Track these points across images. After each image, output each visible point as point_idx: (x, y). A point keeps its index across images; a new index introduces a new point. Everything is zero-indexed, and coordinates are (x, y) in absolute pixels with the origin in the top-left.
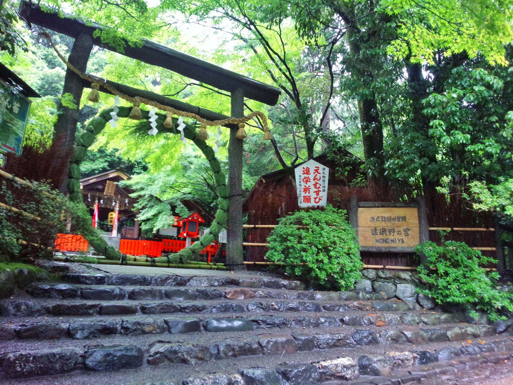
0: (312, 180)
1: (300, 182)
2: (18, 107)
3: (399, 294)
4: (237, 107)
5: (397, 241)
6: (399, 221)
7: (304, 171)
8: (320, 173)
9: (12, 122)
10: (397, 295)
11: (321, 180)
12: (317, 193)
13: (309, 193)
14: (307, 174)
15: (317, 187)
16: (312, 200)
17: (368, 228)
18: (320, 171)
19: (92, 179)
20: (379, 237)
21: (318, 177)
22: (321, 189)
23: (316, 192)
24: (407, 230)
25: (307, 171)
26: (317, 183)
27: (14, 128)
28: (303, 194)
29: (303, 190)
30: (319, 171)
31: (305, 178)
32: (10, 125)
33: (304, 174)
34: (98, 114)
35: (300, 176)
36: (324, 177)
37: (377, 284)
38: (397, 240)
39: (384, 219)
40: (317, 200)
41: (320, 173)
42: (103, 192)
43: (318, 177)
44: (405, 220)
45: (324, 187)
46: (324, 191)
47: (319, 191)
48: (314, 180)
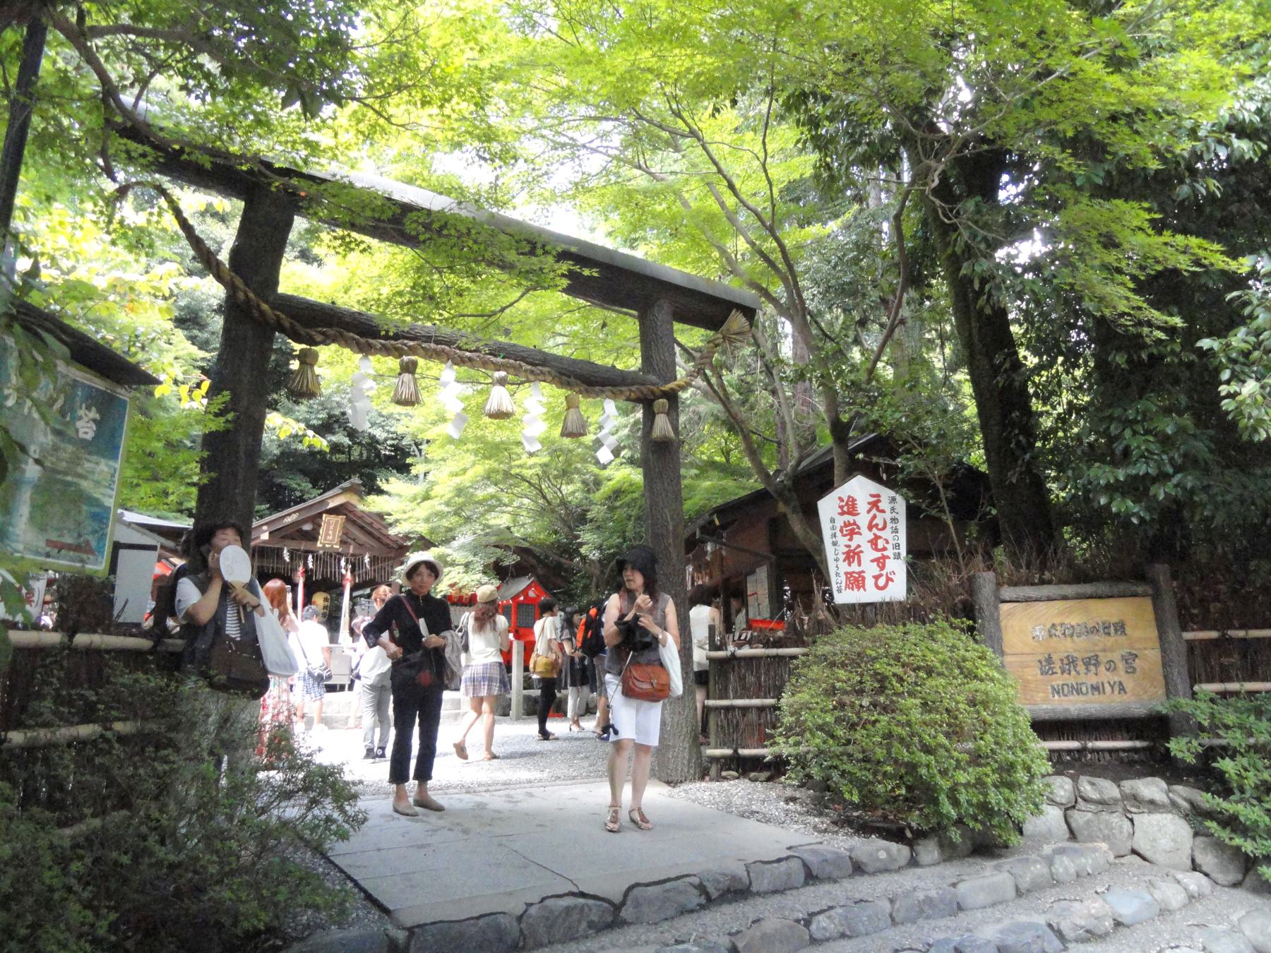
0: (864, 530)
1: (834, 535)
2: (94, 421)
3: (1143, 846)
4: (654, 345)
5: (1108, 689)
6: (1109, 634)
7: (841, 507)
8: (883, 511)
9: (79, 470)
10: (1136, 847)
11: (888, 530)
12: (881, 562)
13: (859, 564)
14: (849, 513)
15: (880, 546)
16: (870, 582)
17: (1029, 658)
18: (884, 505)
19: (289, 515)
20: (1058, 680)
21: (879, 521)
22: (890, 552)
23: (876, 560)
24: (1129, 659)
25: (850, 507)
26: (877, 537)
27: (85, 485)
28: (844, 568)
29: (842, 557)
30: (881, 506)
31: (846, 525)
32: (69, 478)
33: (843, 513)
34: (334, 438)
35: (833, 520)
36: (894, 520)
37: (1079, 818)
38: (1107, 685)
39: (1070, 632)
40: (882, 582)
41: (883, 511)
42: (315, 539)
43: (879, 521)
44: (1124, 633)
45: (897, 546)
46: (897, 556)
47: (885, 557)
48: (870, 528)
